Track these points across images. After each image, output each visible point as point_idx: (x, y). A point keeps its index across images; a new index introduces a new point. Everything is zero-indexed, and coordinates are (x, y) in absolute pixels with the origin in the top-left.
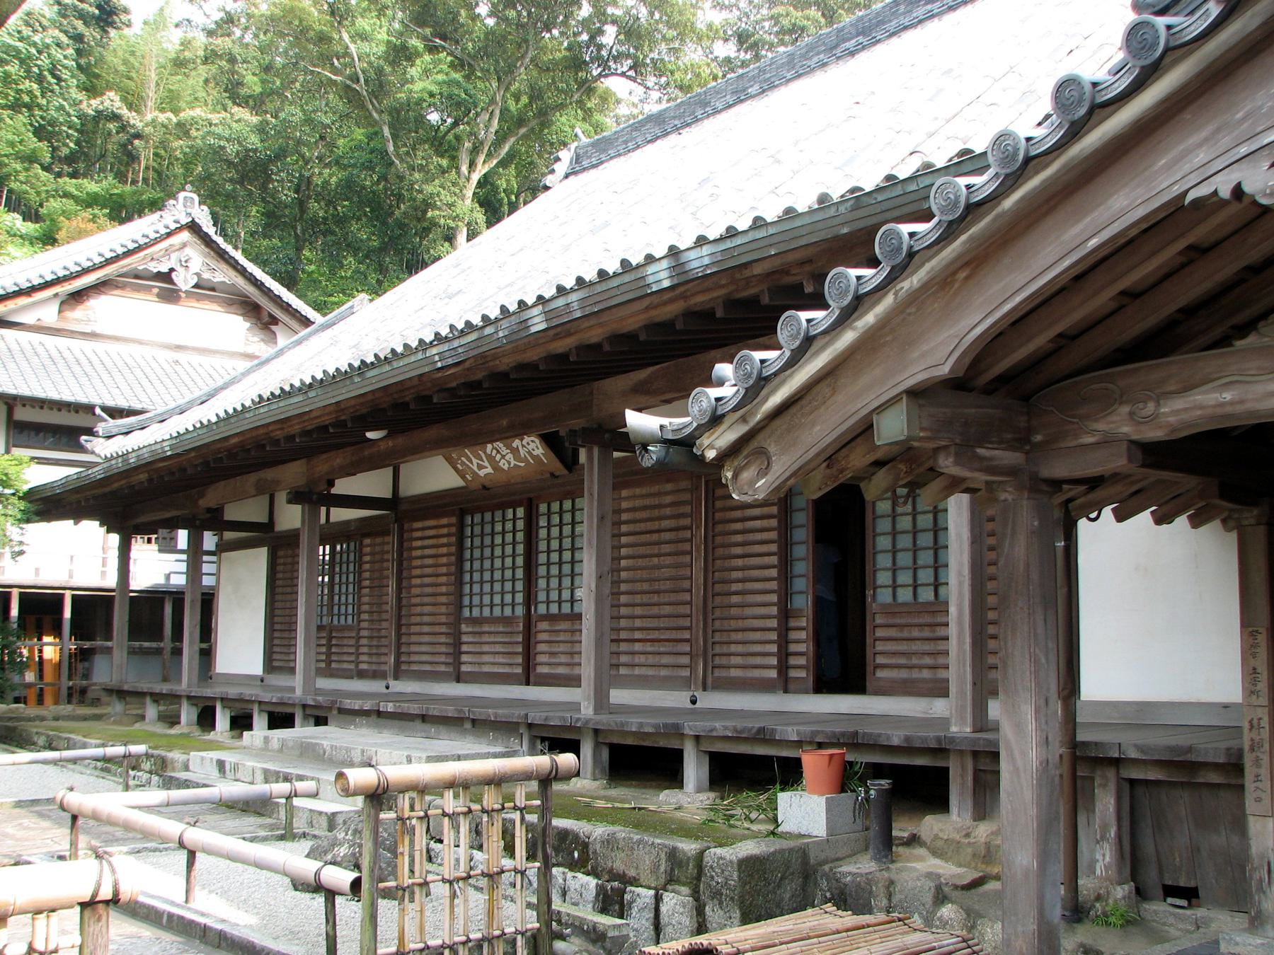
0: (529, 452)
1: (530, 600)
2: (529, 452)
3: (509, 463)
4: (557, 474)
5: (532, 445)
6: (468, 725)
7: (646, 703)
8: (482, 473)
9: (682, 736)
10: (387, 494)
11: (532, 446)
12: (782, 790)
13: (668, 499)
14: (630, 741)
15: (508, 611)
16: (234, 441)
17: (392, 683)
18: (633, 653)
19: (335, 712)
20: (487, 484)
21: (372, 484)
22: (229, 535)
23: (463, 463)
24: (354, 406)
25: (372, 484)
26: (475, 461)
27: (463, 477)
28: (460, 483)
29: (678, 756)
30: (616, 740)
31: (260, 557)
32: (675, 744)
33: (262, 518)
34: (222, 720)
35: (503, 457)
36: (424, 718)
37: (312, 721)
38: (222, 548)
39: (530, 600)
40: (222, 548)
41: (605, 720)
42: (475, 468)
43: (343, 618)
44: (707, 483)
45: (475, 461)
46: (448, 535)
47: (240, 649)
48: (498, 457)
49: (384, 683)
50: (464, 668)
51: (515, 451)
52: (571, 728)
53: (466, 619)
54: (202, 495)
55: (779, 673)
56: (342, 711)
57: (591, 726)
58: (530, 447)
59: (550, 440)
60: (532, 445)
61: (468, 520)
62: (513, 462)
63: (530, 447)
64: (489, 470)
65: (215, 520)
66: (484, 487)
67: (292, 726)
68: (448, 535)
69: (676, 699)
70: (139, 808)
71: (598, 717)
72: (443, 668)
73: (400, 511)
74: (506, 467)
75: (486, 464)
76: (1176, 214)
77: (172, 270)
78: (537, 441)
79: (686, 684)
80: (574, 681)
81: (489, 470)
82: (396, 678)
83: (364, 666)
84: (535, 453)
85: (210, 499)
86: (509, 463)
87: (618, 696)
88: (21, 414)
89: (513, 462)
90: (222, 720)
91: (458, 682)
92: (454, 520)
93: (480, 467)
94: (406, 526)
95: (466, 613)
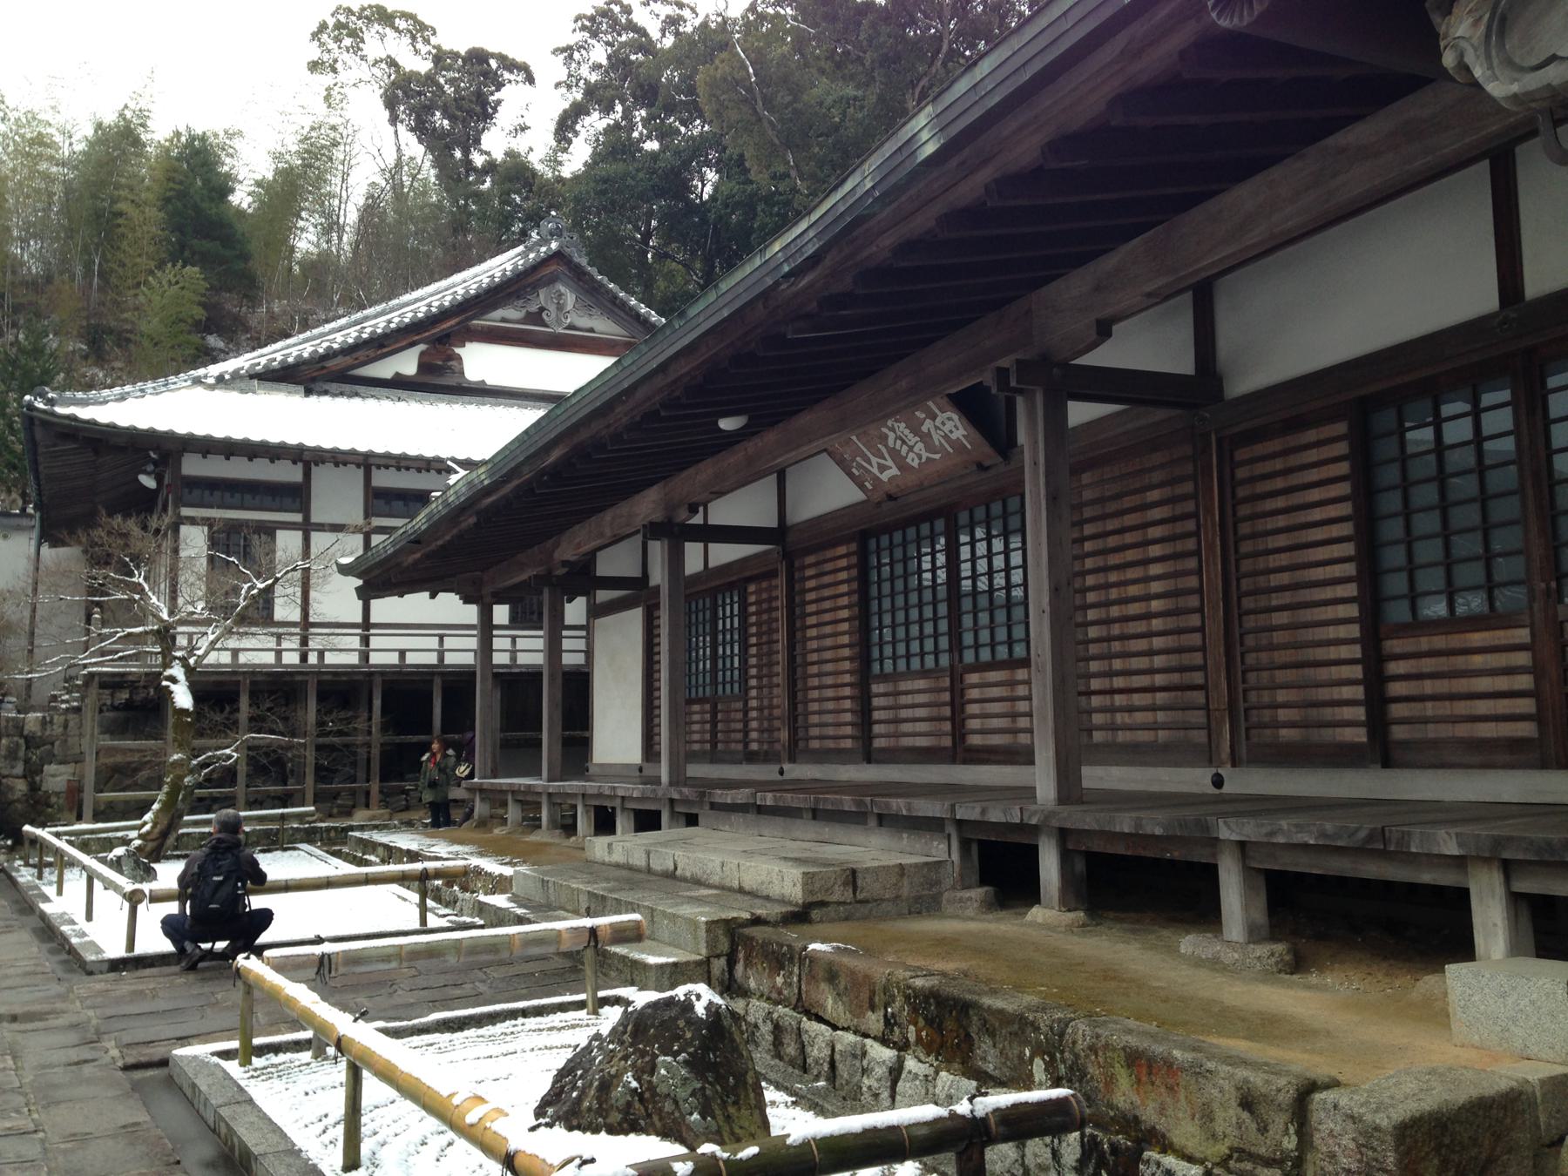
0: (946, 437)
1: (956, 646)
2: (946, 437)
3: (920, 457)
4: (987, 463)
5: (949, 425)
6: (873, 822)
7: (1143, 787)
8: (885, 477)
9: (1215, 842)
10: (772, 522)
11: (950, 427)
12: (570, 601)
13: (1157, 477)
14: (1120, 849)
15: (930, 661)
16: (555, 455)
17: (786, 767)
18: (1112, 692)
19: (707, 807)
20: (893, 490)
21: (747, 507)
22: (603, 596)
23: (860, 466)
24: (688, 373)
25: (747, 507)
26: (874, 460)
27: (861, 487)
28: (856, 495)
29: (1210, 873)
30: (1097, 846)
31: (634, 619)
32: (1200, 856)
33: (634, 571)
34: (583, 823)
35: (911, 449)
36: (816, 814)
37: (683, 820)
38: (595, 611)
39: (956, 646)
40: (595, 611)
41: (1083, 819)
42: (875, 470)
43: (728, 687)
44: (1219, 441)
45: (874, 460)
46: (847, 568)
47: (617, 735)
48: (905, 449)
49: (777, 768)
50: (879, 743)
51: (926, 438)
52: (1022, 827)
53: (878, 677)
54: (557, 545)
55: (1372, 734)
56: (713, 806)
57: (1055, 823)
58: (946, 429)
59: (971, 405)
60: (949, 425)
61: (873, 544)
62: (925, 455)
63: (946, 429)
64: (894, 471)
65: (582, 579)
66: (890, 497)
67: (659, 828)
68: (847, 568)
69: (1194, 779)
70: (63, 1012)
71: (1065, 810)
72: (848, 744)
73: (788, 543)
74: (915, 464)
75: (890, 463)
76: (821, 1112)
77: (542, 309)
78: (955, 417)
79: (1208, 756)
80: (1024, 756)
81: (894, 471)
82: (792, 760)
83: (754, 746)
84: (953, 436)
85: (568, 550)
86: (920, 457)
87: (1095, 777)
88: (383, 479)
89: (925, 455)
90: (583, 823)
91: (869, 762)
92: (853, 547)
93: (882, 468)
94: (797, 564)
95: (876, 667)
